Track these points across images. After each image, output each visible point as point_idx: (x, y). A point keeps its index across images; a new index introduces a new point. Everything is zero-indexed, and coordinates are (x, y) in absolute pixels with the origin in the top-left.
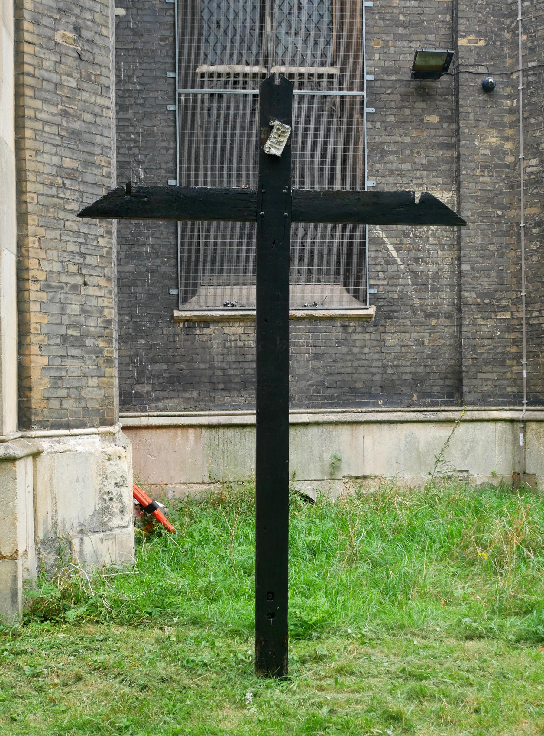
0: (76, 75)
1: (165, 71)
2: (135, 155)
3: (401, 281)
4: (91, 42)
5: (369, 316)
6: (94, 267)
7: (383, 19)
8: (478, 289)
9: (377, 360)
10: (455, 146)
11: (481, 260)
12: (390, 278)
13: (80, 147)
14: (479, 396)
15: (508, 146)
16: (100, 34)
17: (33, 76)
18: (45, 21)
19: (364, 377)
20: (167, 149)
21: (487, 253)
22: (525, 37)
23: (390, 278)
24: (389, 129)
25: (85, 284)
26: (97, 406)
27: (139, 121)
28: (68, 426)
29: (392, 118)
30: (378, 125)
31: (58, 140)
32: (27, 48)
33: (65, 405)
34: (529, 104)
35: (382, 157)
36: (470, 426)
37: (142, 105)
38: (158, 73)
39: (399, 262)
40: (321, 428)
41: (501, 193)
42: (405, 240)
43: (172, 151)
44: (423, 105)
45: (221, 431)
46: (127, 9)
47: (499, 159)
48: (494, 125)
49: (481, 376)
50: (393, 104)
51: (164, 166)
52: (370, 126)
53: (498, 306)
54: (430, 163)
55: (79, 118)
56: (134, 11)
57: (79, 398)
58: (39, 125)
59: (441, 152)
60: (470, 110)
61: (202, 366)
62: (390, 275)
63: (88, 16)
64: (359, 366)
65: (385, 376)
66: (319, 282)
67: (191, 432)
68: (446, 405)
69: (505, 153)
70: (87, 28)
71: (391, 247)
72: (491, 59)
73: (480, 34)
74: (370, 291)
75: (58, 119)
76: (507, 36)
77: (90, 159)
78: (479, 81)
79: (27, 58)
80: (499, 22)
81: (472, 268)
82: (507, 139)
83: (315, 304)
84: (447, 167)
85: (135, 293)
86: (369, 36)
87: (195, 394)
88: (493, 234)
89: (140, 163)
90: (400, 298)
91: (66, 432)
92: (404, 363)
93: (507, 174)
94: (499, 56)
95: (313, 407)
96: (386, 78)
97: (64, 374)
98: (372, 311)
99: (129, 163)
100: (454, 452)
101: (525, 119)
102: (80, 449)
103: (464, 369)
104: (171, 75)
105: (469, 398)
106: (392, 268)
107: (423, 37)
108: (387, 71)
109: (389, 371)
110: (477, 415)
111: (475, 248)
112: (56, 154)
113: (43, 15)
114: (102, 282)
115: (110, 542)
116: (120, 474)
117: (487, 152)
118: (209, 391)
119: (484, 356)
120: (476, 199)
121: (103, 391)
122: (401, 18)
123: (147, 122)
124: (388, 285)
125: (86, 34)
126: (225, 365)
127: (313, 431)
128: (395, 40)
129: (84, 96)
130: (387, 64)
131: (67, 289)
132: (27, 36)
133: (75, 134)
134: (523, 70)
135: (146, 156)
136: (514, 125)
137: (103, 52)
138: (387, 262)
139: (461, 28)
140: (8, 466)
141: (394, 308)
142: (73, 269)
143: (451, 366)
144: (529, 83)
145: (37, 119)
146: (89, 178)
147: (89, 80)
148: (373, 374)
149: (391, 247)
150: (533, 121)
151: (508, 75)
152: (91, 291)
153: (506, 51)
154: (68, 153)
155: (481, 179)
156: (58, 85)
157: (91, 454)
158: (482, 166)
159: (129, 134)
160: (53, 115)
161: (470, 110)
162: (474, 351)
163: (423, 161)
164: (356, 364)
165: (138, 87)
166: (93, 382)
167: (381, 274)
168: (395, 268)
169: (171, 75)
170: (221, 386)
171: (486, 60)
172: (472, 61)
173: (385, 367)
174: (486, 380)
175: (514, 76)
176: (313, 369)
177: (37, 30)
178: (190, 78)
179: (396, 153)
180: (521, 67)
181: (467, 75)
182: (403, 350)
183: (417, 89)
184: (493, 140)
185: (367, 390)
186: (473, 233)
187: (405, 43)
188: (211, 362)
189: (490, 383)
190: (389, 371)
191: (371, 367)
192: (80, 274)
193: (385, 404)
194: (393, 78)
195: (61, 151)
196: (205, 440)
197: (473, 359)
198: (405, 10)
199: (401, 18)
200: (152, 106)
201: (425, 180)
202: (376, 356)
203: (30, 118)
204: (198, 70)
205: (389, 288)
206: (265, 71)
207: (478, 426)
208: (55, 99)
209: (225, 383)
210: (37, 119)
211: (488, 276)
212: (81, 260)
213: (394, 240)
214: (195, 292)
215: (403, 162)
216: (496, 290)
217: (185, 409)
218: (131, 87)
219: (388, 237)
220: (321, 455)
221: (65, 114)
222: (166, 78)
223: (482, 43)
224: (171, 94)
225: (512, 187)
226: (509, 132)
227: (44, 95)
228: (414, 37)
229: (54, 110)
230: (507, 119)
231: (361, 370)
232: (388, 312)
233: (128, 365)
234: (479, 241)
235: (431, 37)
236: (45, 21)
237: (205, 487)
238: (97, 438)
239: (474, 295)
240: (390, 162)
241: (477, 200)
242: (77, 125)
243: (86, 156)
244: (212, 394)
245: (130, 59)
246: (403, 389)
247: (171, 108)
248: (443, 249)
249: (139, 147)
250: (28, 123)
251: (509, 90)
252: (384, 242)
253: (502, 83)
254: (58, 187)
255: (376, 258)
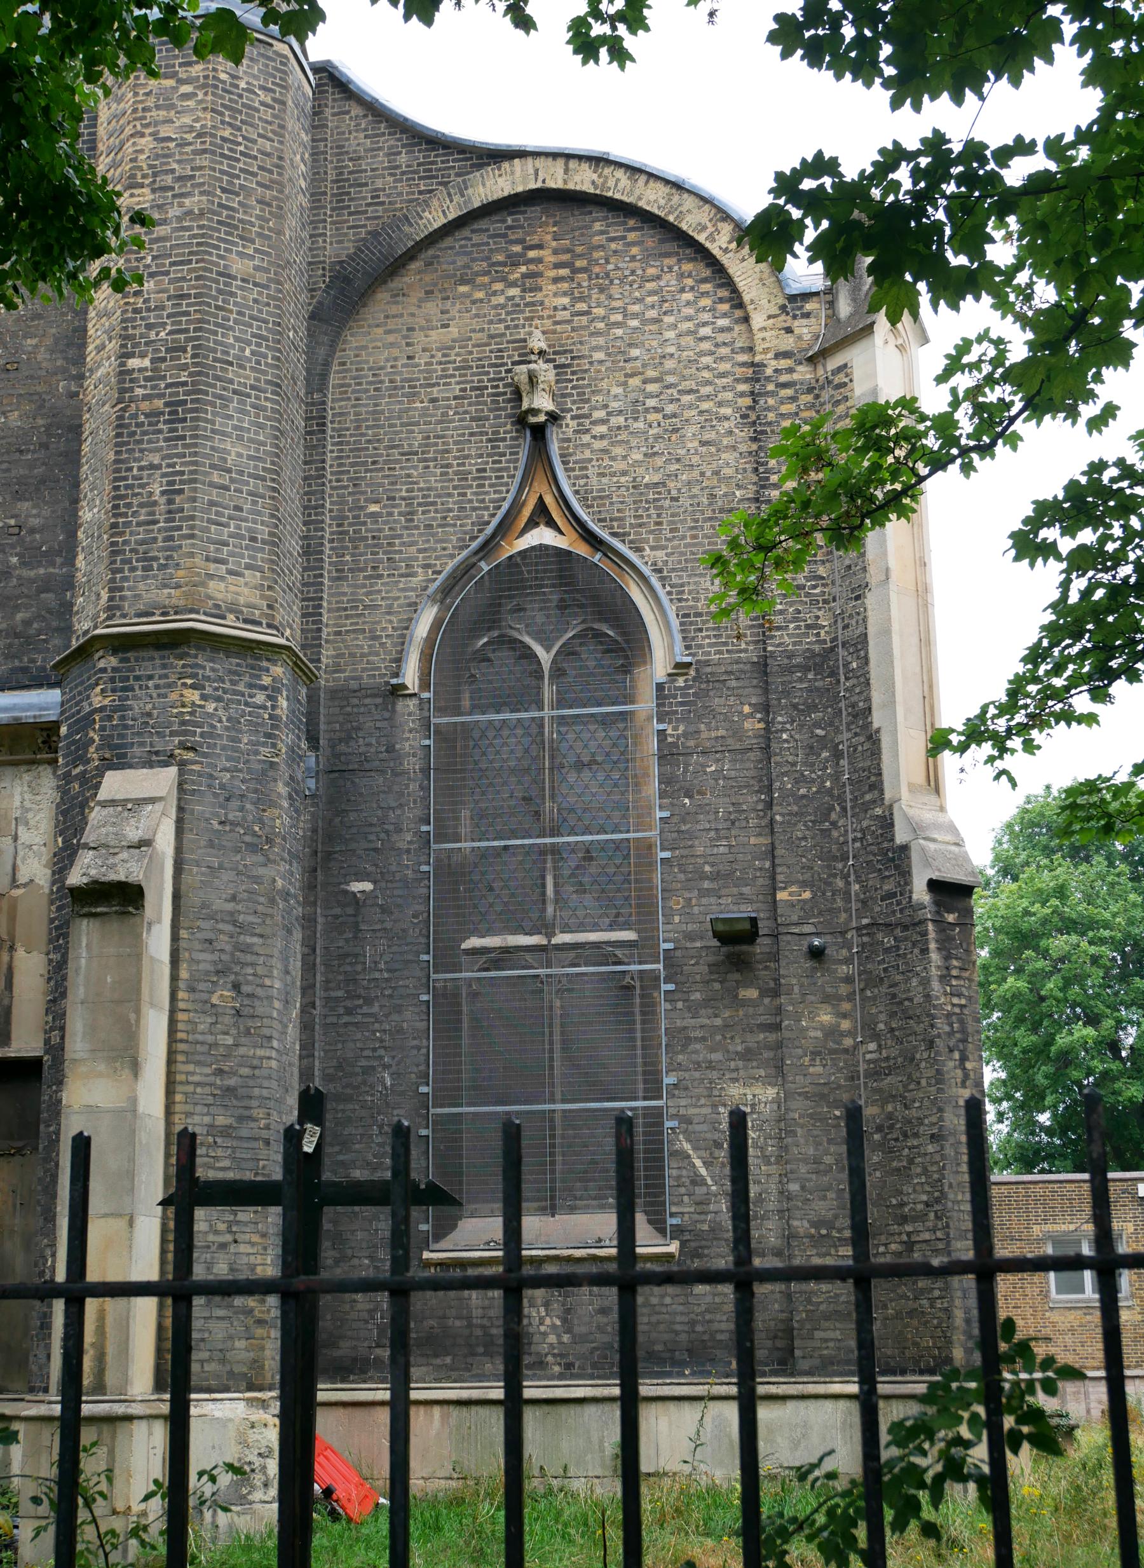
0: (233, 1031)
1: (418, 953)
2: (381, 1058)
3: (712, 1207)
4: (251, 996)
5: (670, 1256)
6: (246, 1224)
7: (684, 872)
8: (813, 1216)
9: (682, 1314)
10: (777, 1027)
11: (814, 1177)
12: (697, 1204)
13: (235, 1102)
14: (817, 1362)
15: (846, 1025)
16: (263, 986)
17: (187, 1041)
18: (201, 986)
19: (666, 1337)
20: (419, 1048)
21: (822, 1167)
22: (857, 887)
23: (697, 1204)
24: (693, 1010)
25: (236, 1242)
26: (245, 1370)
27: (387, 1016)
28: (210, 1390)
29: (697, 996)
30: (680, 1005)
31: (210, 1100)
32: (181, 1016)
33: (206, 1368)
34: (865, 972)
35: (685, 1046)
36: (802, 1405)
37: (391, 996)
38: (410, 957)
39: (710, 1182)
40: (601, 1406)
41: (839, 1087)
42: (717, 1153)
43: (424, 1051)
44: (737, 976)
45: (474, 1409)
46: (375, 882)
47: (835, 1042)
48: (827, 999)
49: (818, 1334)
50: (698, 977)
51: (415, 1070)
52: (669, 1007)
53: (839, 1239)
54: (748, 1050)
55: (235, 1074)
56: (383, 884)
57: (223, 1361)
58: (190, 1088)
59: (762, 1036)
60: (794, 981)
61: (458, 1323)
62: (698, 1199)
63: (250, 970)
64: (659, 1323)
65: (693, 1336)
66: (586, 1209)
67: (437, 1411)
68: (776, 1376)
69: (843, 1034)
70: (248, 983)
71: (698, 1163)
72: (820, 913)
73: (804, 884)
74: (671, 1221)
75: (211, 1079)
76: (840, 883)
77: (246, 1113)
78: (805, 944)
79: (180, 1026)
80: (829, 867)
81: (803, 1188)
82: (845, 1016)
83: (600, 1240)
84: (771, 1054)
85: (377, 1230)
86: (667, 895)
87: (448, 1360)
88: (830, 1141)
89: (386, 1067)
90: (712, 1230)
91: (206, 1396)
92: (718, 1317)
93: (845, 1062)
94: (830, 910)
95: (599, 1378)
96: (688, 945)
97: (206, 1335)
98: (673, 1247)
99: (373, 1068)
100: (779, 1440)
101: (862, 990)
102: (218, 1414)
103: (796, 1325)
104: (425, 957)
105: (804, 1365)
106: (700, 1191)
107: (735, 890)
108: (690, 936)
109: (699, 1328)
110: (811, 1389)
111: (805, 1161)
112: (208, 1114)
113: (198, 981)
114: (256, 1238)
115: (248, 1517)
116: (264, 1443)
117: (819, 1034)
118: (465, 1356)
119: (823, 1307)
120: (806, 1096)
121: (252, 1354)
122: (707, 868)
123: (395, 1017)
124: (696, 1212)
125: (246, 989)
126: (485, 1322)
127: (591, 1410)
128: (700, 896)
129: (242, 1051)
130: (690, 927)
131: (214, 1248)
132: (181, 1005)
133: (230, 1091)
134: (858, 929)
135: (393, 1057)
136: (850, 998)
137: (265, 1003)
138: (694, 1183)
139: (780, 878)
140: (126, 1424)
141: (704, 1243)
142: (222, 1227)
143: (782, 1321)
144: (863, 945)
145: (188, 1083)
146: (244, 1133)
147: (248, 1032)
148: (677, 1333)
149: (698, 1163)
150: (869, 994)
151: (843, 933)
152: (242, 1248)
153: (840, 903)
154: (221, 1111)
155: (811, 1070)
156: (215, 1045)
157: (231, 1420)
158: (812, 1053)
159: (374, 1032)
160: (207, 1075)
161: (794, 981)
162: (809, 1301)
163: (739, 1048)
164: (654, 1319)
165: (386, 975)
166: (240, 1344)
167: (686, 1198)
168: (704, 1190)
169: (425, 957)
170: (481, 1350)
171: (814, 916)
172: (795, 918)
173: (693, 1323)
174: (826, 1340)
175: (849, 936)
176: (598, 1327)
177: (192, 996)
178: (448, 958)
179: (704, 1039)
180: (854, 924)
181: (789, 937)
182: (717, 1300)
183: (729, 956)
184: (826, 1018)
185: (668, 1355)
186: (802, 1141)
187: (713, 900)
188: (469, 1318)
189: (831, 1344)
190: (699, 1328)
191: (674, 1323)
192: (230, 1232)
193: (693, 1374)
194: (698, 944)
195: (213, 1110)
196: (453, 1421)
197: (807, 1311)
198: (711, 859)
199: (707, 868)
200: (402, 997)
201: (742, 1072)
202: (681, 1308)
203: (181, 1083)
204: (463, 946)
205: (696, 1217)
206: (545, 942)
207: (812, 1404)
208: (209, 1059)
209: (485, 1346)
210: (188, 1083)
211: (824, 1198)
212: (232, 1218)
213: (703, 1153)
214: (455, 1226)
215: (713, 1050)
216: (836, 1217)
217: (437, 1380)
218: (377, 975)
219: (694, 1149)
220: (601, 1442)
221: (220, 1072)
222: (419, 962)
223: (807, 895)
224: (424, 981)
225: (852, 1078)
226: (846, 1006)
227: (198, 1058)
228: (723, 892)
229: (208, 1070)
230: (844, 989)
231: (662, 1327)
232: (696, 1249)
233: (367, 1322)
234: (811, 1151)
235: (746, 890)
236: (201, 986)
237: (453, 1484)
238: (242, 1404)
239: (806, 1224)
240: (696, 1052)
241: (807, 1098)
242: (232, 1082)
243: (241, 1111)
244: (470, 1360)
245: (377, 942)
246: (718, 1352)
247: (424, 998)
248: (768, 1163)
249: (385, 1048)
250: (179, 1088)
251: (844, 952)
252: (689, 1156)
253: (835, 944)
254: (209, 1146)
255: (679, 1177)
